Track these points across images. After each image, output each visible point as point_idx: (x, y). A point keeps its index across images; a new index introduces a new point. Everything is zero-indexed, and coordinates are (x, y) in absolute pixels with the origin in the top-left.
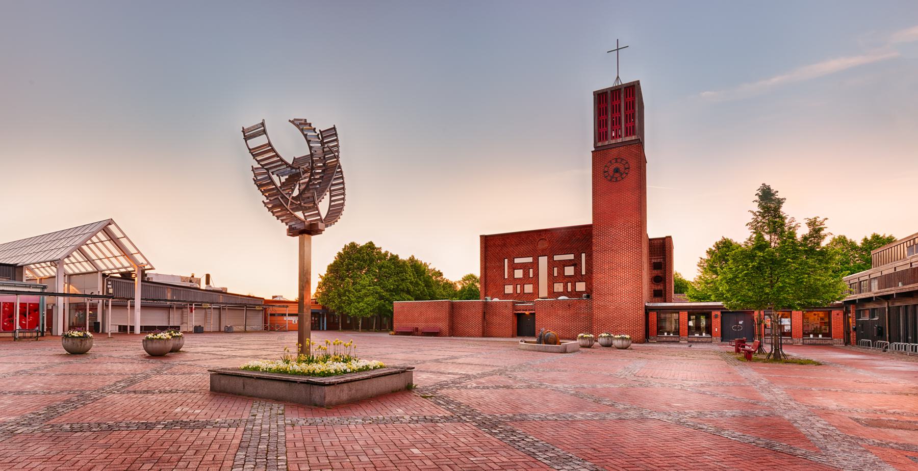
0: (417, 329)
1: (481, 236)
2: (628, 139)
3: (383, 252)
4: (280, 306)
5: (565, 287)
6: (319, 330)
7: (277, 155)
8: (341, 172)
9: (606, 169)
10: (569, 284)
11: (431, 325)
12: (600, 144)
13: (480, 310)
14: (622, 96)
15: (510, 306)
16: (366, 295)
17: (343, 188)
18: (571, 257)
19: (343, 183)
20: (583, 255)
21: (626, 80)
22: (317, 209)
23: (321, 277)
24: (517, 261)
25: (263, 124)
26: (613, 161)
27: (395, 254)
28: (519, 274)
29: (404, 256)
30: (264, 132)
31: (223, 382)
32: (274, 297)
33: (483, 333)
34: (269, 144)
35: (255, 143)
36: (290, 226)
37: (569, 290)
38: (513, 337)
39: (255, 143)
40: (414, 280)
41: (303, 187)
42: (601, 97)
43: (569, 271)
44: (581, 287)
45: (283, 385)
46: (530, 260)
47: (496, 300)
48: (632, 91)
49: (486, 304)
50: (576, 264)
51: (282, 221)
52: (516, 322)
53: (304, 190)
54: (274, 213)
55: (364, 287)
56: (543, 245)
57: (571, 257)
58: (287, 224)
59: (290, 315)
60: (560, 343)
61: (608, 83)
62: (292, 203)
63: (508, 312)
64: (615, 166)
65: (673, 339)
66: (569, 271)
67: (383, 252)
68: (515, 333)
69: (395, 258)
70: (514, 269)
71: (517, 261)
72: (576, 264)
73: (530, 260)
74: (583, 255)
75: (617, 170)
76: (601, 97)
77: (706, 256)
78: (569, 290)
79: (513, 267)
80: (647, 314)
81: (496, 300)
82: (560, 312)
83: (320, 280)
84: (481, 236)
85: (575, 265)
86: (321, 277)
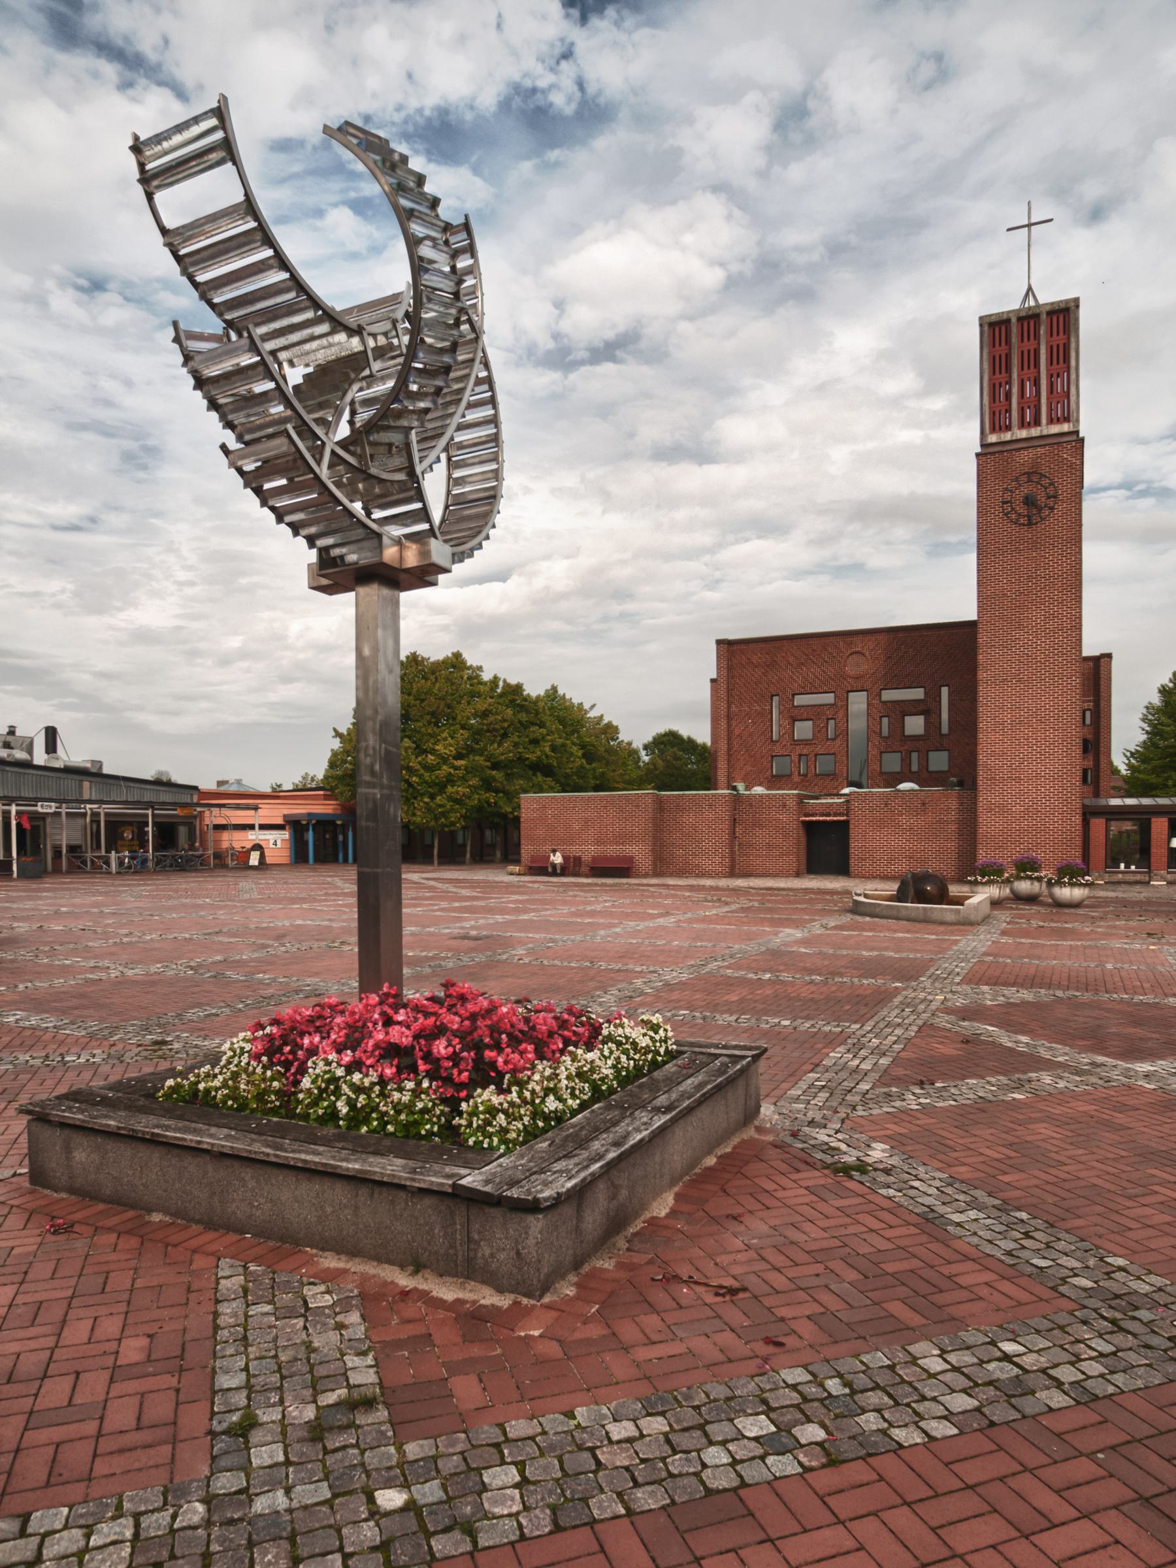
0: (578, 859)
1: (719, 642)
2: (1055, 429)
3: (486, 676)
4: (238, 807)
5: (906, 761)
6: (335, 860)
7: (281, 262)
8: (489, 381)
9: (1007, 497)
10: (915, 756)
11: (613, 850)
12: (993, 438)
13: (723, 813)
14: (1042, 331)
15: (792, 803)
16: (450, 780)
17: (495, 439)
18: (918, 694)
19: (494, 421)
20: (945, 691)
21: (1047, 296)
22: (420, 496)
23: (338, 734)
24: (799, 700)
25: (220, 113)
26: (1024, 478)
27: (513, 681)
28: (804, 730)
29: (535, 689)
30: (228, 151)
31: (79, 1156)
32: (220, 783)
33: (732, 867)
34: (249, 207)
35: (184, 201)
36: (323, 552)
37: (915, 768)
38: (798, 875)
39: (184, 201)
40: (544, 743)
41: (363, 416)
42: (995, 330)
43: (915, 725)
44: (939, 761)
45: (340, 1193)
46: (829, 698)
47: (759, 790)
48: (1064, 316)
49: (737, 799)
50: (927, 709)
51: (295, 528)
52: (803, 841)
53: (371, 426)
54: (264, 498)
55: (444, 760)
56: (854, 667)
57: (918, 694)
58: (311, 541)
59: (263, 827)
60: (959, 901)
61: (1011, 303)
62: (336, 459)
63: (789, 820)
64: (1025, 490)
65: (1138, 877)
66: (915, 725)
67: (486, 676)
68: (803, 867)
69: (515, 691)
70: (794, 720)
71: (799, 700)
72: (927, 709)
73: (829, 698)
74: (945, 691)
75: (1029, 501)
76: (995, 330)
77: (1156, 700)
78: (915, 768)
79: (794, 716)
80: (1086, 824)
81: (759, 790)
82: (903, 819)
83: (336, 744)
84: (719, 642)
85: (926, 713)
86: (338, 734)
